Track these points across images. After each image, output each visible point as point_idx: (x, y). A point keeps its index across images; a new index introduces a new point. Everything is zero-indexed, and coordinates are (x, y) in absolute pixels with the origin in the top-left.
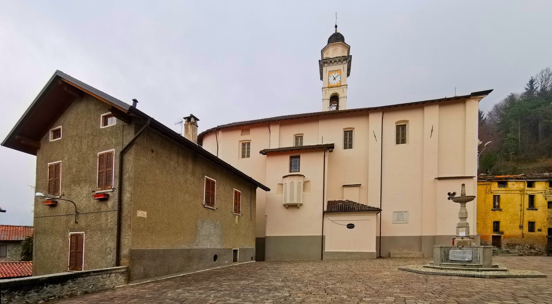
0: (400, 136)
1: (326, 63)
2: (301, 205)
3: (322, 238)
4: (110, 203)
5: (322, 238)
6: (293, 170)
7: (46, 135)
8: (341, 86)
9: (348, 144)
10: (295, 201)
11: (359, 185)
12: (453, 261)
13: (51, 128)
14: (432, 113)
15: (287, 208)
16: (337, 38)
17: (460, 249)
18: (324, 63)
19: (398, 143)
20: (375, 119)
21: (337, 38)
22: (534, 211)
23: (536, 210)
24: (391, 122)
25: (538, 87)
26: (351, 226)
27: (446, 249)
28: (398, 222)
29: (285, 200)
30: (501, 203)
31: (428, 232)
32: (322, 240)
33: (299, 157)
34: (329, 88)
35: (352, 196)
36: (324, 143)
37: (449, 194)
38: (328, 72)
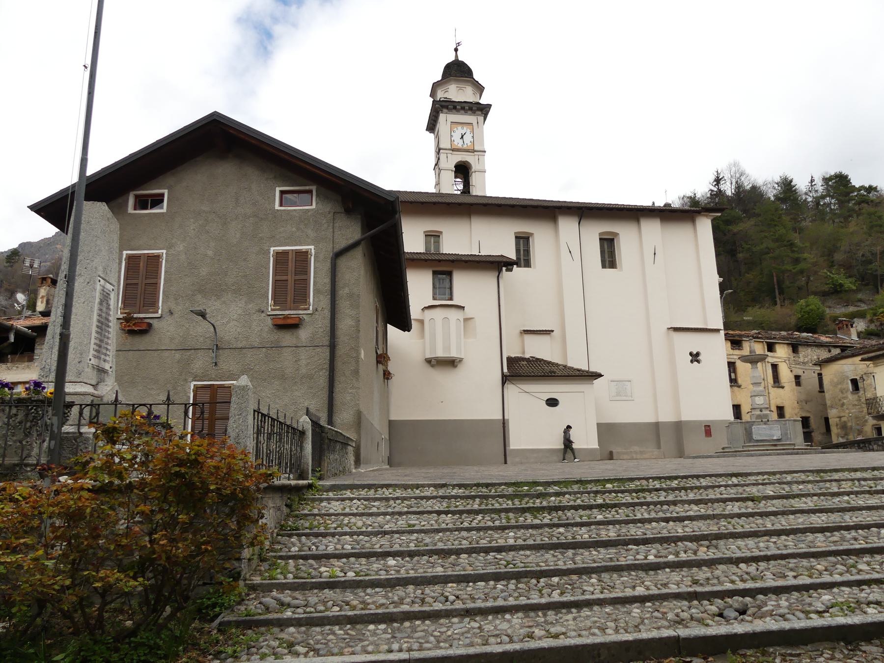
0: (607, 256)
1: (447, 107)
2: (461, 360)
3: (504, 423)
4: (304, 334)
5: (504, 423)
6: (438, 296)
7: (120, 200)
8: (474, 151)
9: (524, 259)
10: (454, 354)
11: (548, 332)
12: (758, 441)
13: (133, 190)
14: (651, 229)
15: (433, 366)
16: (457, 71)
17: (765, 424)
18: (443, 107)
19: (604, 266)
20: (568, 226)
21: (457, 71)
22: (781, 390)
23: (783, 387)
24: (593, 231)
25: (728, 189)
26: (552, 402)
27: (747, 425)
28: (618, 398)
29: (433, 348)
30: (738, 375)
31: (666, 416)
32: (504, 427)
33: (450, 274)
34: (453, 150)
35: (538, 349)
36: (484, 253)
37: (692, 362)
38: (449, 123)
